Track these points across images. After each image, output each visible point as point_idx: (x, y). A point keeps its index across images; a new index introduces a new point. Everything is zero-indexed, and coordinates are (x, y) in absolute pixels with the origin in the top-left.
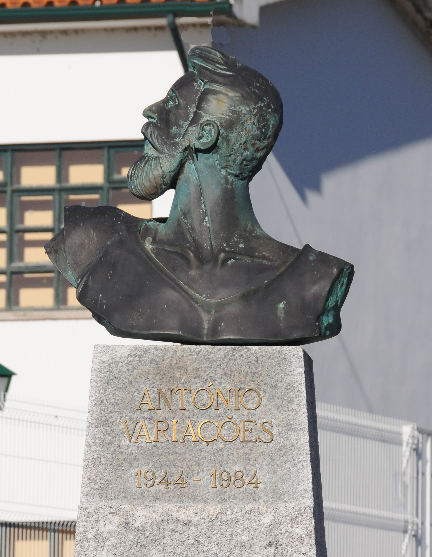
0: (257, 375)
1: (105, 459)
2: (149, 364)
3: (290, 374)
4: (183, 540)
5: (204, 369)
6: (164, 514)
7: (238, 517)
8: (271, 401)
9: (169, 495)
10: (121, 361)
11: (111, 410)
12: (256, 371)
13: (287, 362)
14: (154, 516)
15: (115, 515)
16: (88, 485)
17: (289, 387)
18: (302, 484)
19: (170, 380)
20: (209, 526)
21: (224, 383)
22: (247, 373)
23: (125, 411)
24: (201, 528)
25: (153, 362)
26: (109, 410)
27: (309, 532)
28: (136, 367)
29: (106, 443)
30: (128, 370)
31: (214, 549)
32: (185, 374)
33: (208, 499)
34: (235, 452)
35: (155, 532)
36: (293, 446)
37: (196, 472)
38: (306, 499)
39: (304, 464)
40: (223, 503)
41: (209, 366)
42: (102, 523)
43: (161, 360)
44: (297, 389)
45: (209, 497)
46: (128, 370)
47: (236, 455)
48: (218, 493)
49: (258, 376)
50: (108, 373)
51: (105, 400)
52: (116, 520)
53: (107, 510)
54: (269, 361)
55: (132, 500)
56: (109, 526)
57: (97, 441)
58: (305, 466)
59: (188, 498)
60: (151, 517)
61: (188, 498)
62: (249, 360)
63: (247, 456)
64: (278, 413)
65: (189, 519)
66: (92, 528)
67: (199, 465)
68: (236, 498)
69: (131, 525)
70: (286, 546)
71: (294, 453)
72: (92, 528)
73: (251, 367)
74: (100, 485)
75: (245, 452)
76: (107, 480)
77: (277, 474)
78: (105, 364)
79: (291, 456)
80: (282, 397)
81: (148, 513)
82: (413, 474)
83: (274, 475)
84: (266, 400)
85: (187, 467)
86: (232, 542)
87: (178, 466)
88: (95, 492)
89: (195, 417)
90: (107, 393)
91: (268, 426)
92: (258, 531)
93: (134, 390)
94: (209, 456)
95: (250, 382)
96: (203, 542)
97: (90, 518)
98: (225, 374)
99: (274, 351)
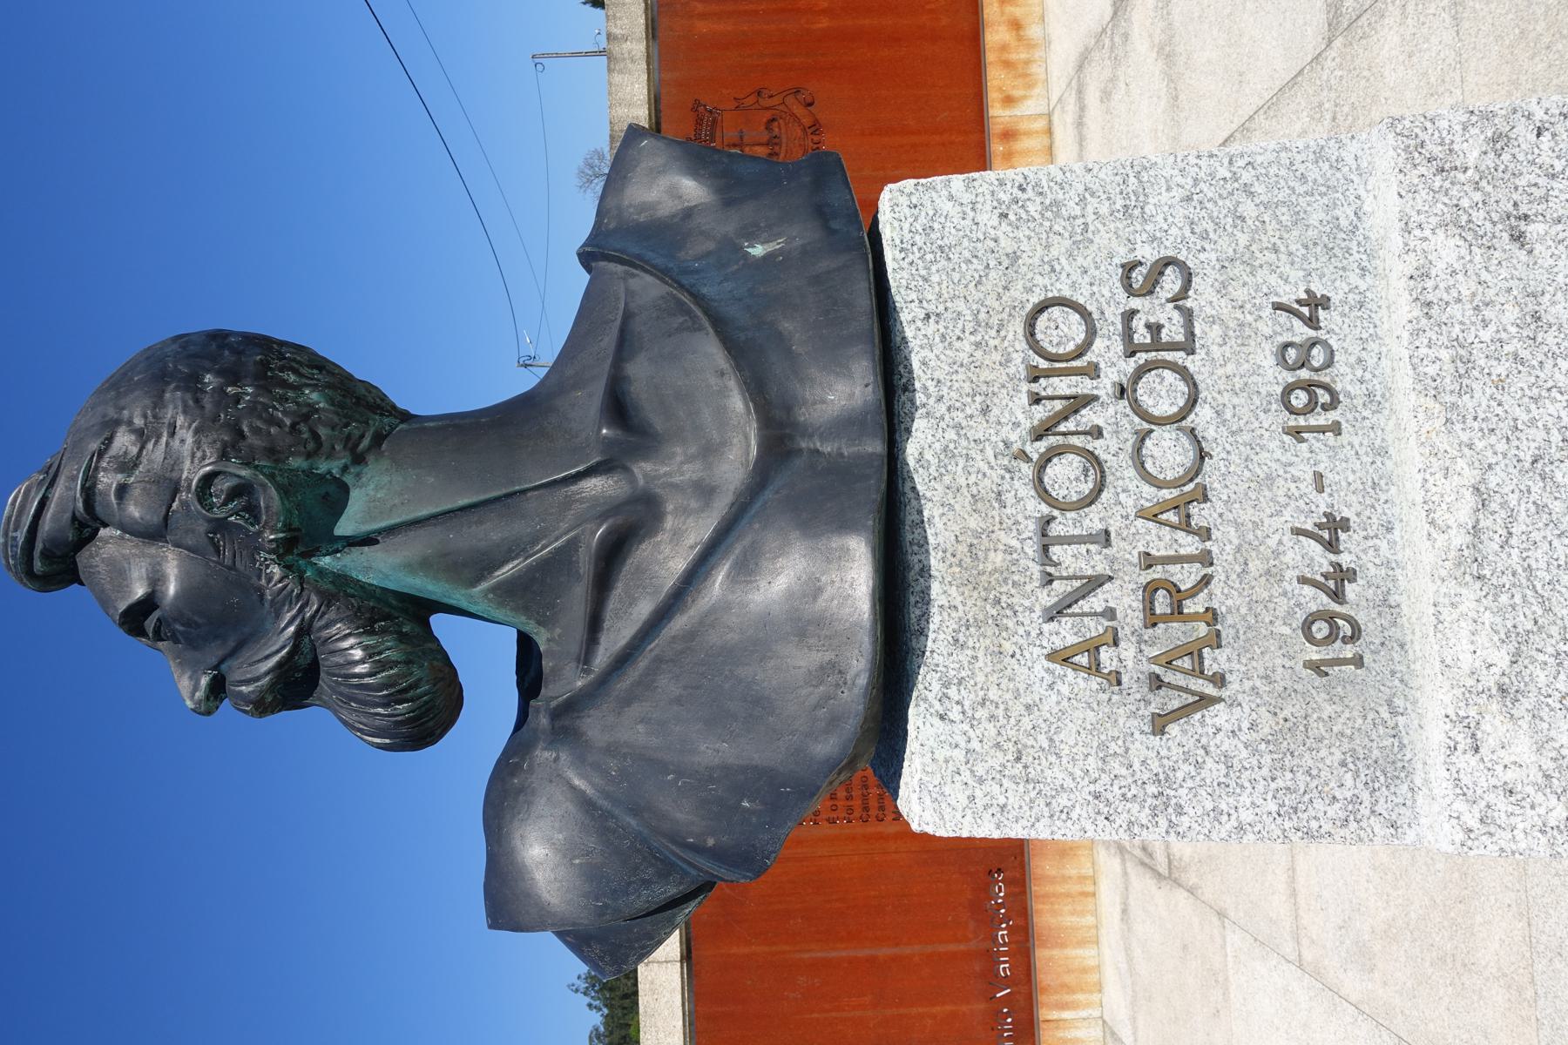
0: (982, 316)
1: (1278, 774)
2: (970, 652)
3: (972, 214)
4: (1533, 509)
5: (972, 479)
6: (1458, 574)
7: (1443, 339)
8: (1058, 268)
9: (1370, 565)
10: (963, 744)
11: (1122, 764)
12: (969, 318)
13: (936, 226)
14: (1468, 605)
15: (1479, 735)
16: (1364, 824)
17: (1012, 217)
18: (1302, 168)
19: (1014, 584)
20: (1481, 430)
21: (1012, 412)
22: (978, 345)
23: (1121, 721)
24: (1489, 453)
25: (962, 639)
26: (1124, 771)
27: (1474, 119)
28: (981, 693)
29: (1227, 775)
30: (992, 717)
31: (1552, 410)
32: (993, 536)
33: (1372, 446)
34: (1220, 372)
35: (1518, 599)
36: (1189, 199)
37: (1293, 486)
38: (1344, 154)
39: (1241, 163)
40: (1378, 398)
41: (962, 462)
42: (1510, 776)
43: (954, 614)
44: (1015, 191)
45: (1365, 442)
46: (992, 717)
47: (1230, 368)
48: (1350, 416)
49: (984, 310)
50: (1006, 782)
51: (1092, 787)
52: (1494, 726)
53: (1466, 761)
54: (935, 278)
55: (1397, 682)
56: (1518, 750)
57: (1223, 806)
58: (1247, 159)
59: (1373, 507)
60: (1473, 614)
61: (1373, 507)
62: (937, 339)
63: (1231, 333)
64: (1094, 247)
65: (1468, 494)
66: (1533, 807)
67: (1270, 479)
68: (1360, 361)
69: (1507, 680)
70: (1516, 188)
71: (1210, 195)
72: (1533, 807)
73: (958, 332)
74: (1361, 786)
75: (1219, 340)
76: (1343, 764)
77: (1279, 242)
78: (978, 793)
79: (1220, 203)
80: (1044, 236)
81: (1463, 624)
82: (573, 788)
83: (1283, 249)
84: (1058, 286)
85: (1279, 513)
86: (1524, 354)
87: (1280, 542)
88: (1382, 800)
89: (1123, 497)
90: (1069, 783)
91: (1138, 276)
92: (1485, 276)
93: (1054, 698)
94: (1242, 448)
95: (1003, 333)
96: (1533, 445)
97: (1496, 814)
98: (985, 411)
99: (905, 264)
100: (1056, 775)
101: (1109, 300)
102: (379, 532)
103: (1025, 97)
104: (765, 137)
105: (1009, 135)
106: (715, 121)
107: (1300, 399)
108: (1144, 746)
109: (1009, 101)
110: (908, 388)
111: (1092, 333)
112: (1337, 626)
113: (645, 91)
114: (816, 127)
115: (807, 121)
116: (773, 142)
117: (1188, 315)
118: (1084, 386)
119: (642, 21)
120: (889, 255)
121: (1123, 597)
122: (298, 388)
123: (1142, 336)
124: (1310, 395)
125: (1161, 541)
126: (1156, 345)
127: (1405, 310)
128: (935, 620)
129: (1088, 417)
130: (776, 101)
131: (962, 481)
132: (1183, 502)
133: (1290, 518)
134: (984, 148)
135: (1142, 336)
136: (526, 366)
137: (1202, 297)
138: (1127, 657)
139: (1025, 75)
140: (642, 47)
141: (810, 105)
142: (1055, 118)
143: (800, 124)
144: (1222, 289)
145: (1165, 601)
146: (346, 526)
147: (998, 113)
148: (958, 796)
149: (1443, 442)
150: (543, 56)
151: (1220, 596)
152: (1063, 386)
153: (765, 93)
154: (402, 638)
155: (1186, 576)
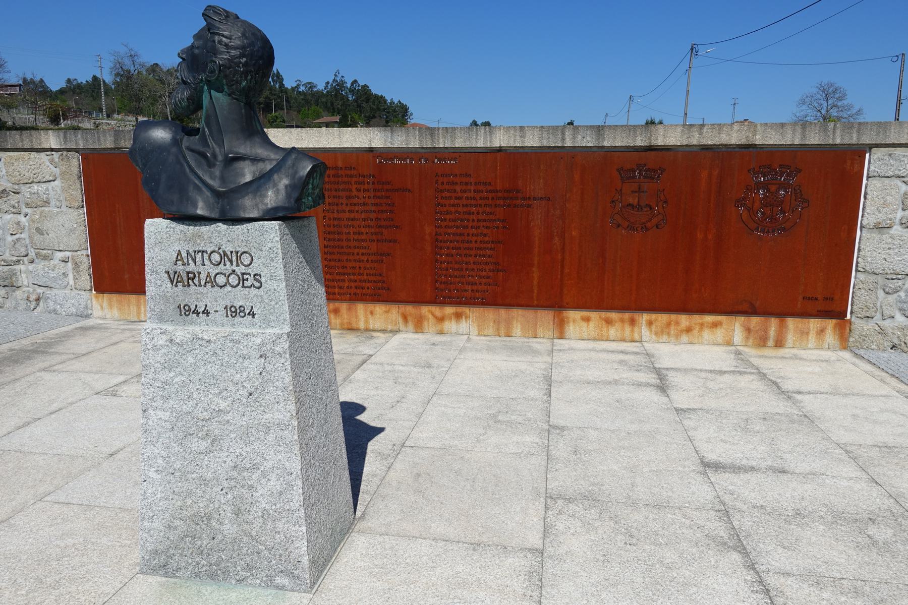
14: (188, 336)
52: (165, 337)
53: (159, 331)
91: (258, 277)
100: (157, 250)
101: (253, 270)
103: (651, 331)
105: (633, 322)
107: (233, 309)
108: (163, 269)
109: (650, 323)
110: (233, 225)
111: (246, 266)
112: (187, 311)
115: (649, 225)
116: (639, 207)
117: (250, 287)
118: (235, 263)
119: (709, 143)
120: (262, 222)
121: (191, 267)
122: (246, 79)
123: (245, 277)
124: (234, 312)
125: (203, 276)
126: (244, 280)
127: (247, 331)
129: (228, 263)
132: (211, 281)
133: (209, 305)
134: (627, 309)
135: (245, 277)
136: (692, 49)
137: (254, 291)
138: (180, 267)
139: (662, 332)
140: (695, 143)
142: (637, 344)
144: (256, 295)
145: (191, 277)
146: (213, 92)
147: (645, 317)
149: (219, 335)
150: (903, 61)
151: (193, 288)
152: (234, 258)
154: (188, 106)
155: (196, 281)
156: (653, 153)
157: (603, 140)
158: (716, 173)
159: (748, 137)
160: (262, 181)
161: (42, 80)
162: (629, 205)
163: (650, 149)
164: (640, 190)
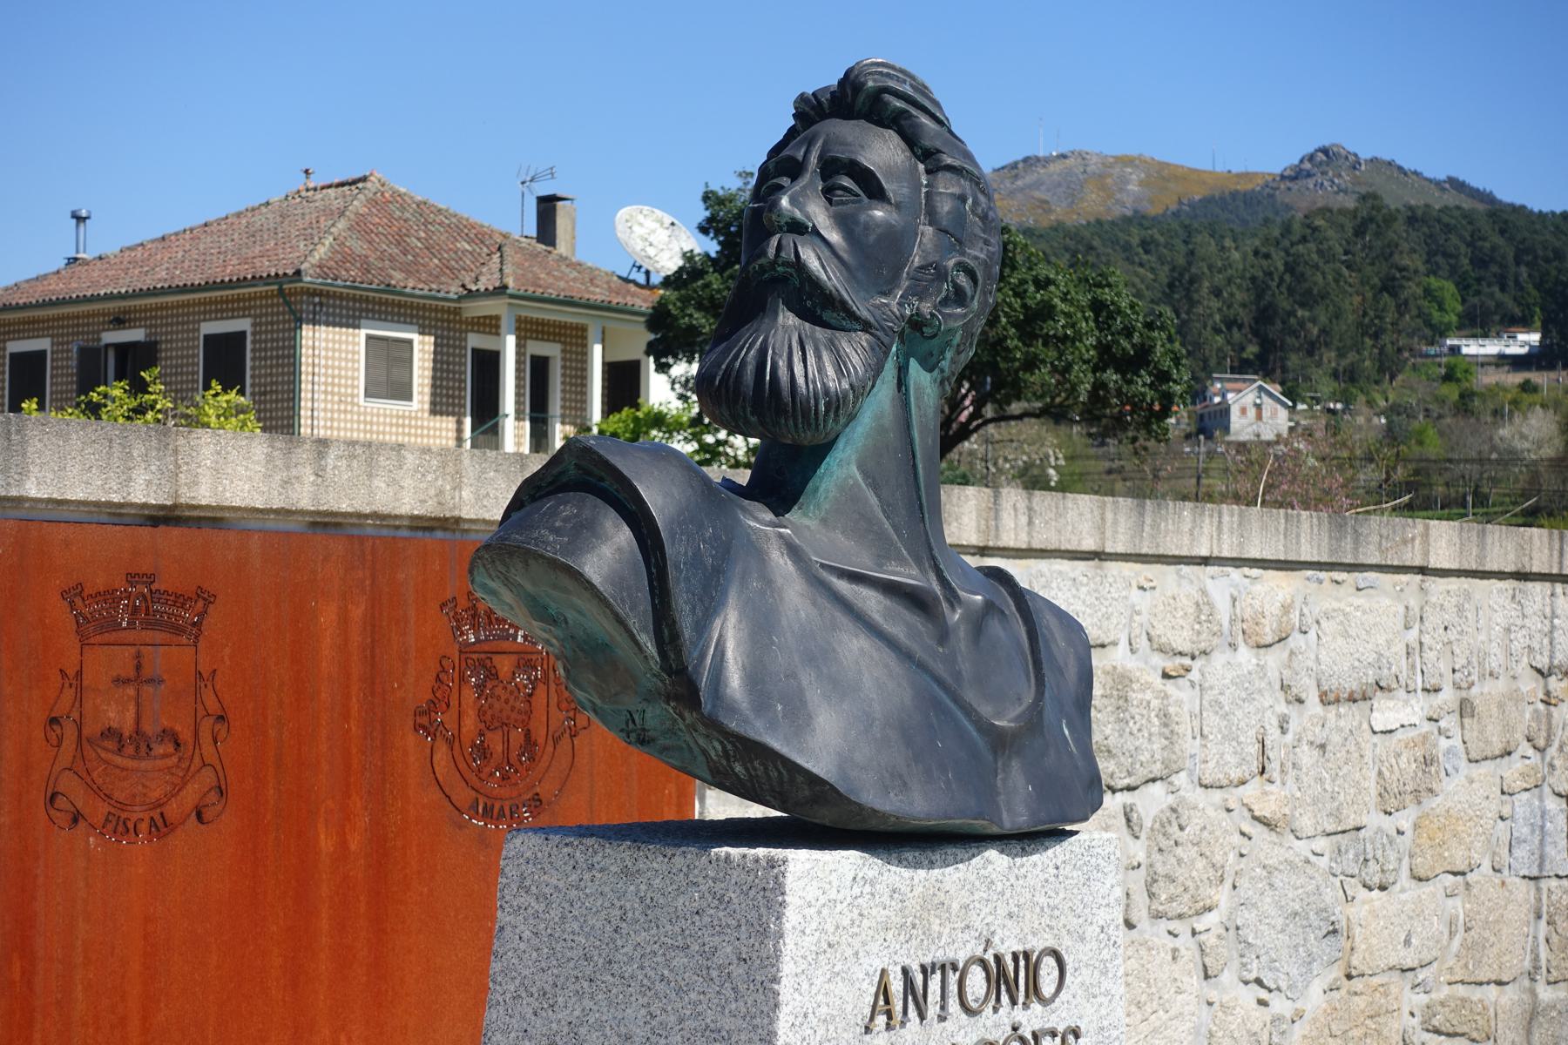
30: (853, 922)
102: (907, 394)
104: (149, 728)
106: (179, 630)
110: (1024, 853)
113: (237, 503)
114: (162, 827)
115: (173, 810)
116: (139, 742)
119: (345, 507)
128: (906, 873)
130: (208, 749)
131: (976, 897)
140: (306, 503)
141: (199, 816)
143: (171, 796)
148: (812, 893)
153: (222, 729)
156: (176, 532)
157: (24, 473)
158: (357, 612)
159: (441, 492)
160: (1043, 655)
161: (1136, 212)
162: (109, 733)
163: (165, 518)
164: (138, 677)
